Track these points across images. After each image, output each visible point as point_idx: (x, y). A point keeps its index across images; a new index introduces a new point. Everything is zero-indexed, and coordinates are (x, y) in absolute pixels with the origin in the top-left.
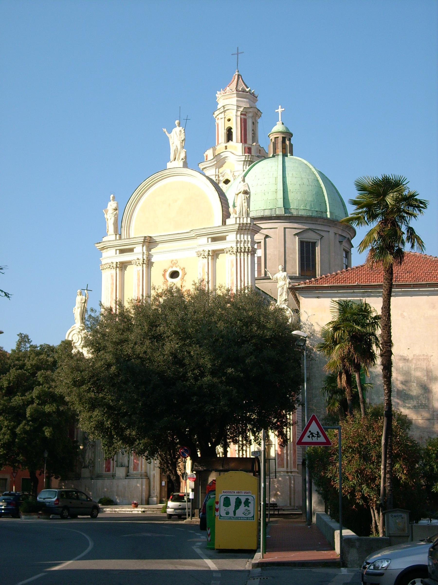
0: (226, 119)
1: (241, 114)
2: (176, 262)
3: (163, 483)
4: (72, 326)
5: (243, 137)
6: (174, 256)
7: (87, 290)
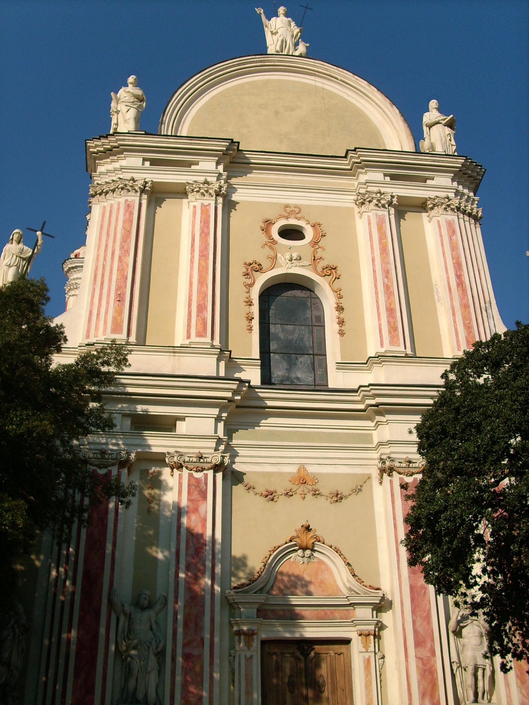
2: (297, 210)
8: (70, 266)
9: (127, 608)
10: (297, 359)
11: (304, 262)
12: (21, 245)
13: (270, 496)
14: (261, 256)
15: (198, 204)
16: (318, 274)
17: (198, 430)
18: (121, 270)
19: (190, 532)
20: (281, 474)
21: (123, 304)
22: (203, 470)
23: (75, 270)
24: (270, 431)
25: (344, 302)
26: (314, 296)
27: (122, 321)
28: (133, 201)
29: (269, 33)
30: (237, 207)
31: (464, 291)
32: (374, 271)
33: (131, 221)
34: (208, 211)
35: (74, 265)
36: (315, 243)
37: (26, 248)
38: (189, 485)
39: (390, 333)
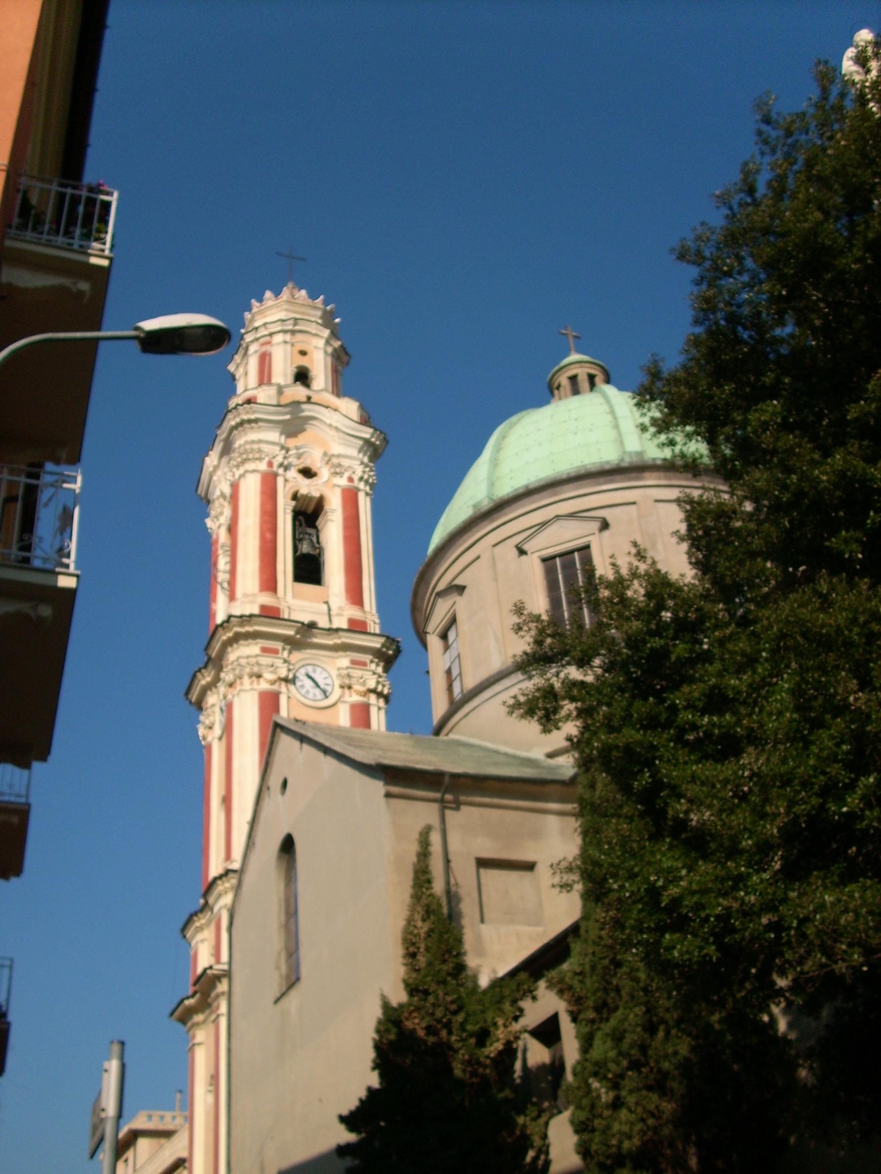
8: (245, 417)
23: (253, 425)
35: (253, 417)
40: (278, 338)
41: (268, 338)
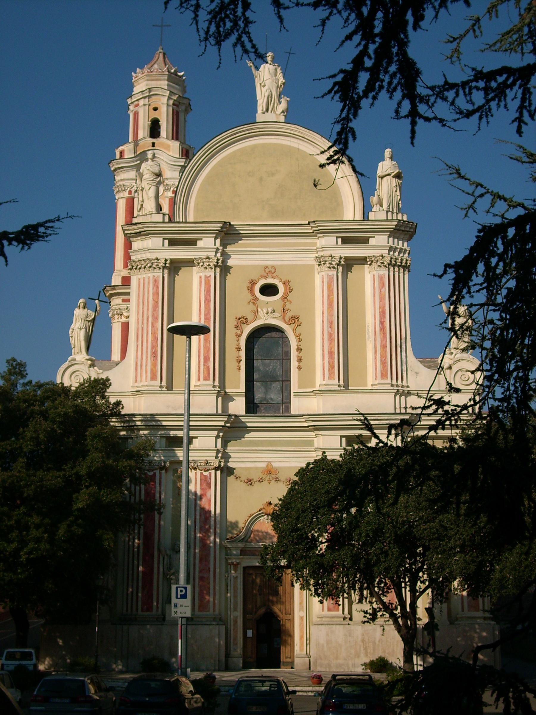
0: (151, 108)
1: (174, 104)
2: (273, 270)
3: (250, 633)
4: (70, 359)
5: (175, 135)
6: (271, 260)
7: (99, 301)
8: (117, 167)
9: (168, 552)
10: (271, 384)
11: (276, 315)
12: (86, 310)
13: (250, 482)
14: (246, 311)
15: (202, 275)
16: (286, 323)
17: (204, 446)
18: (154, 333)
19: (202, 509)
20: (257, 468)
21: (156, 359)
22: (208, 470)
23: (122, 170)
24: (251, 440)
25: (303, 346)
26: (284, 336)
27: (157, 371)
28: (158, 276)
29: (259, 85)
30: (232, 271)
31: (384, 334)
32: (323, 322)
33: (158, 294)
34: (209, 281)
35: (120, 166)
36: (284, 298)
37: (89, 311)
38: (201, 480)
39: (329, 370)
40: (141, 102)
41: (137, 102)
